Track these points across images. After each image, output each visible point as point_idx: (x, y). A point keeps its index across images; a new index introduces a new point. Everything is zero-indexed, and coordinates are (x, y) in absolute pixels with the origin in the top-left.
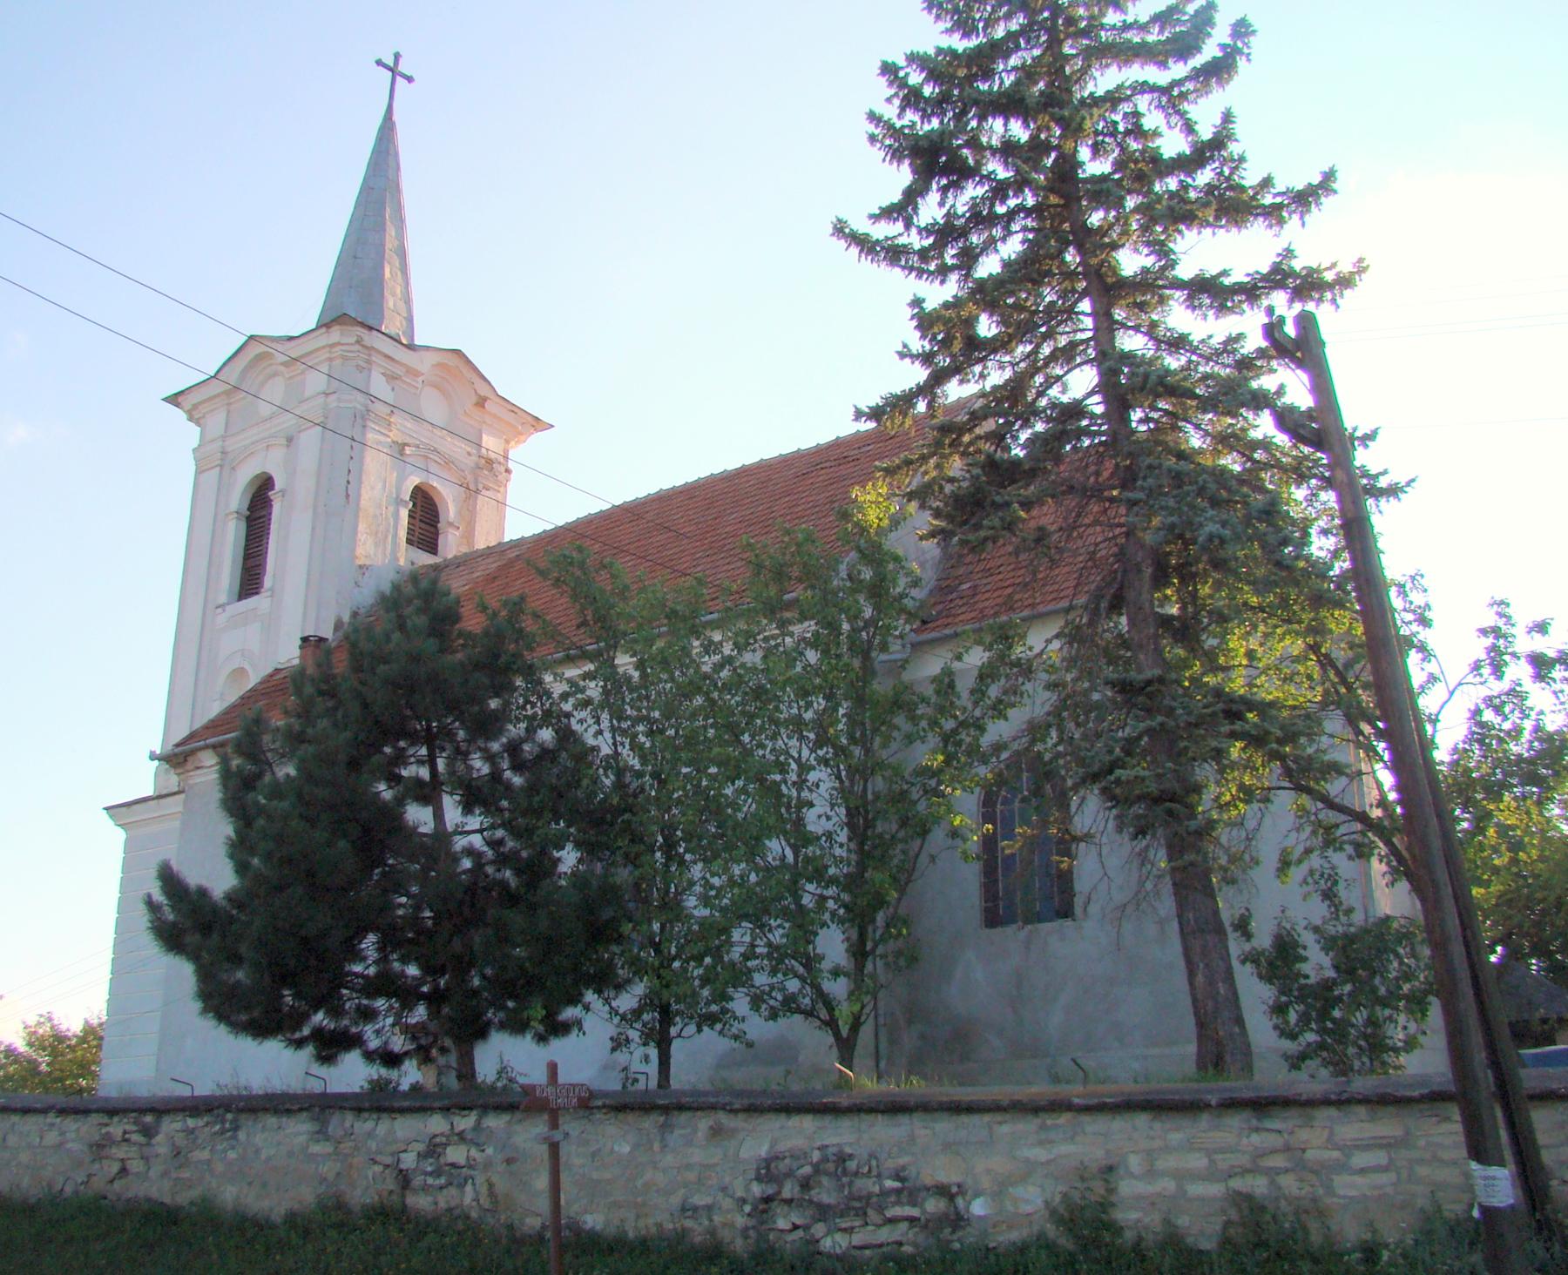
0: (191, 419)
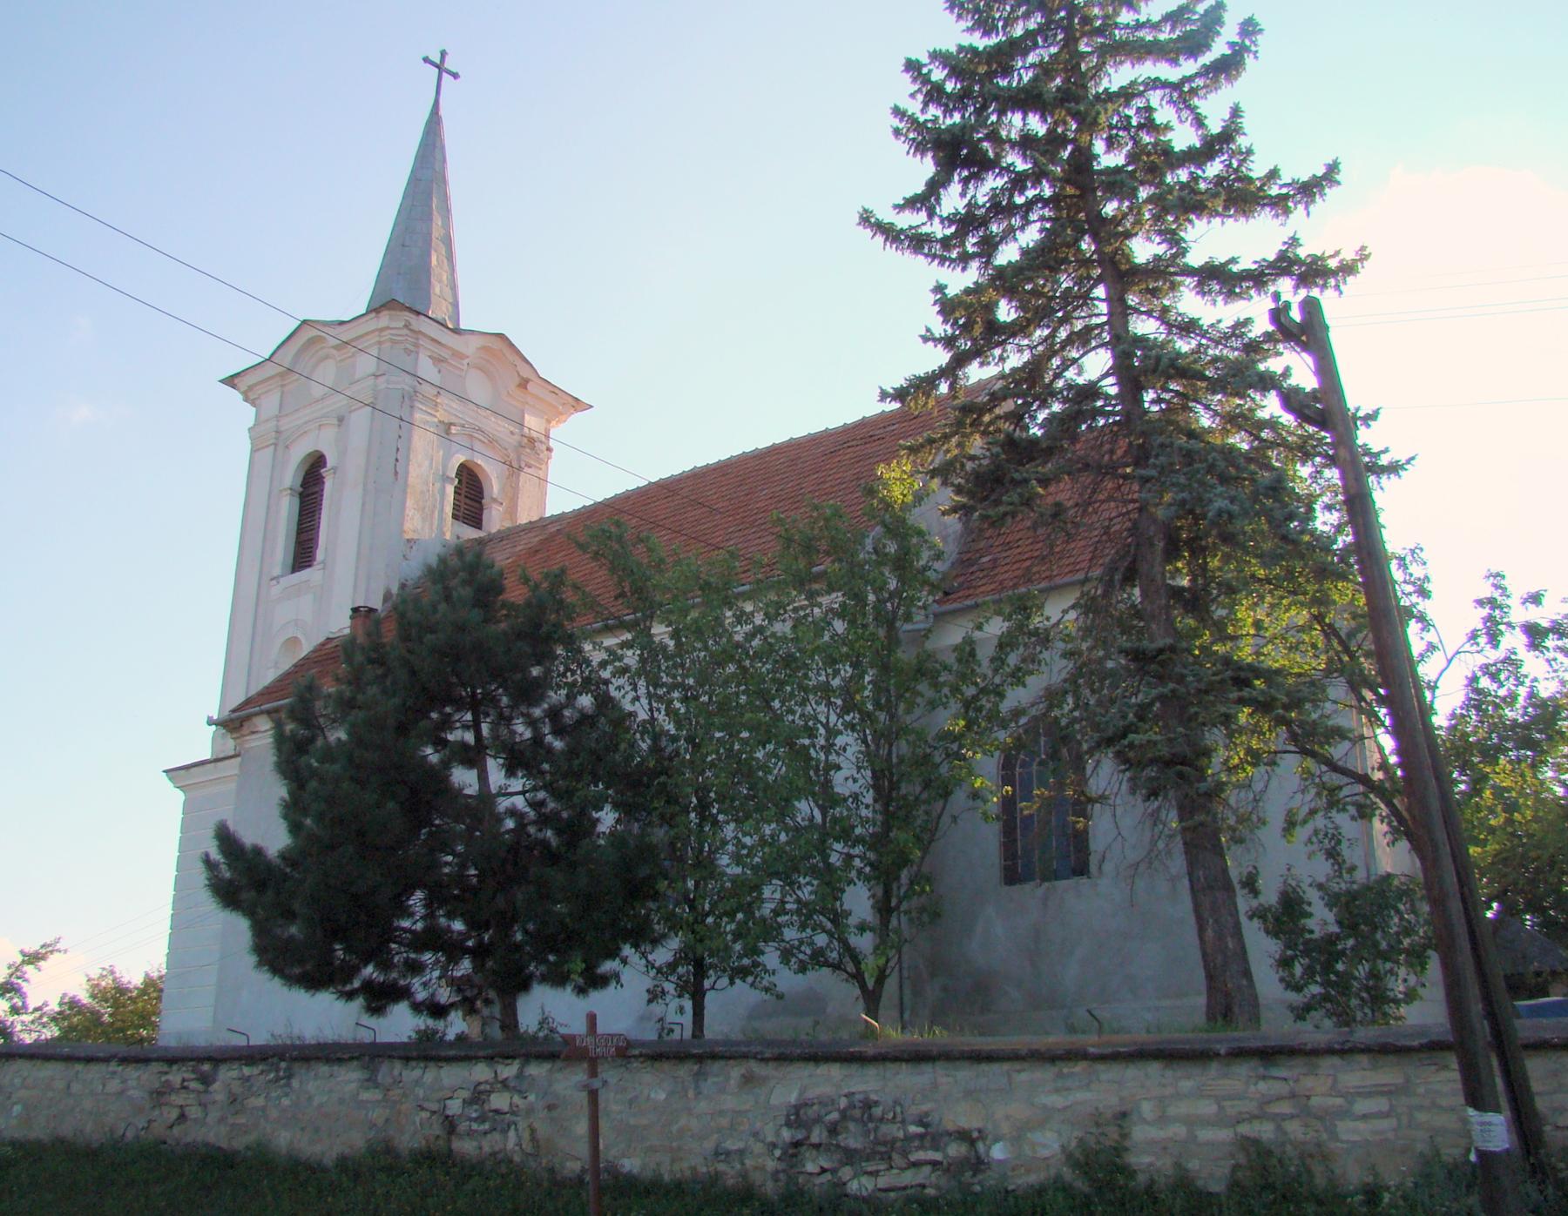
0: (246, 400)
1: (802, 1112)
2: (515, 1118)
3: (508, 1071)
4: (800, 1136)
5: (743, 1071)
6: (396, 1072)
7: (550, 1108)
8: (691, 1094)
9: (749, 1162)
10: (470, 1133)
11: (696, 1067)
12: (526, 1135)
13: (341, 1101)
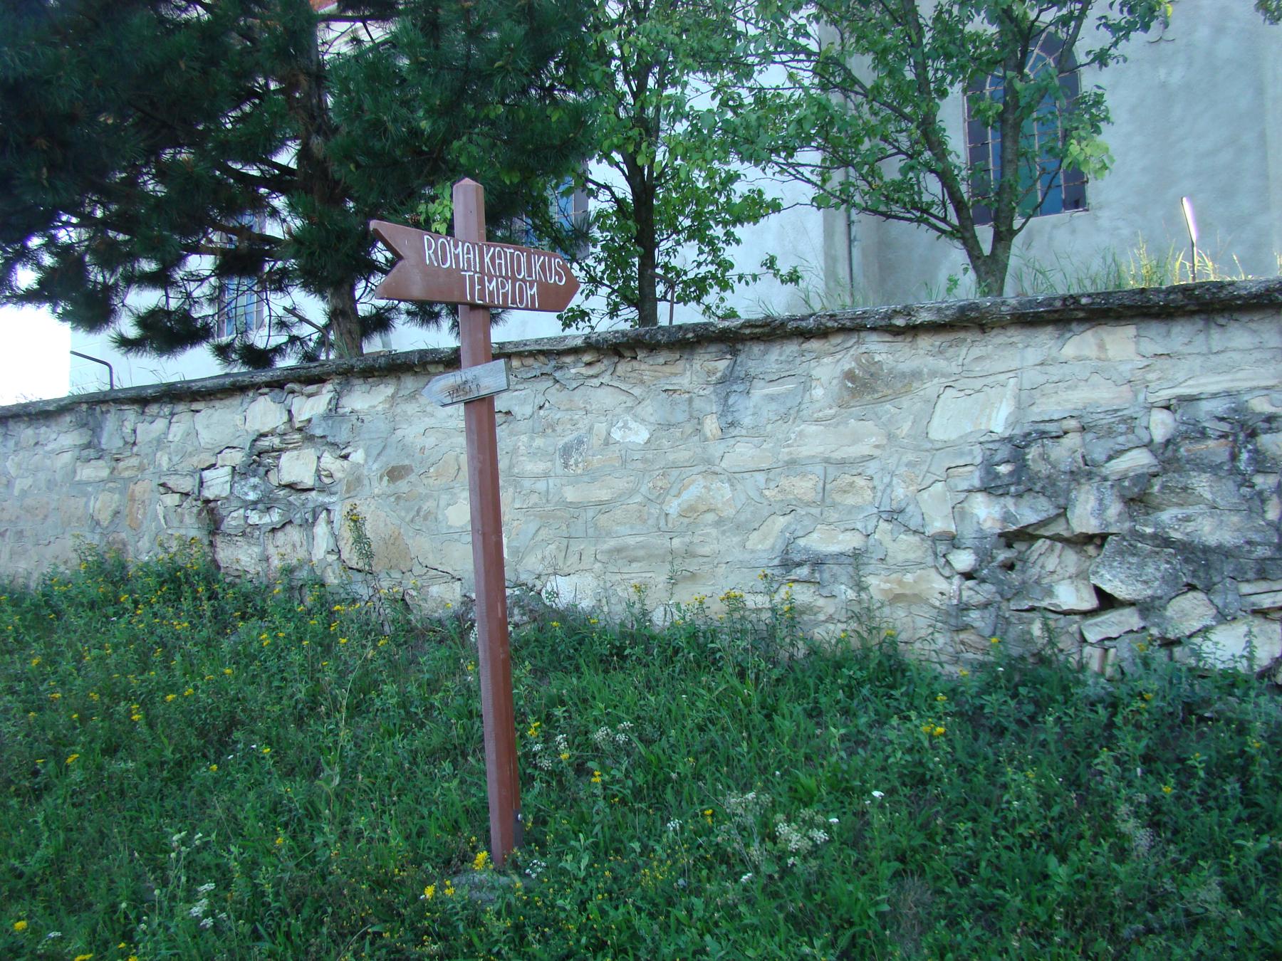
1: (1033, 453)
2: (326, 499)
3: (311, 406)
4: (1028, 513)
5: (847, 363)
6: (128, 428)
7: (394, 474)
8: (711, 426)
9: (877, 584)
10: (247, 532)
11: (722, 365)
12: (347, 535)
13: (51, 485)
